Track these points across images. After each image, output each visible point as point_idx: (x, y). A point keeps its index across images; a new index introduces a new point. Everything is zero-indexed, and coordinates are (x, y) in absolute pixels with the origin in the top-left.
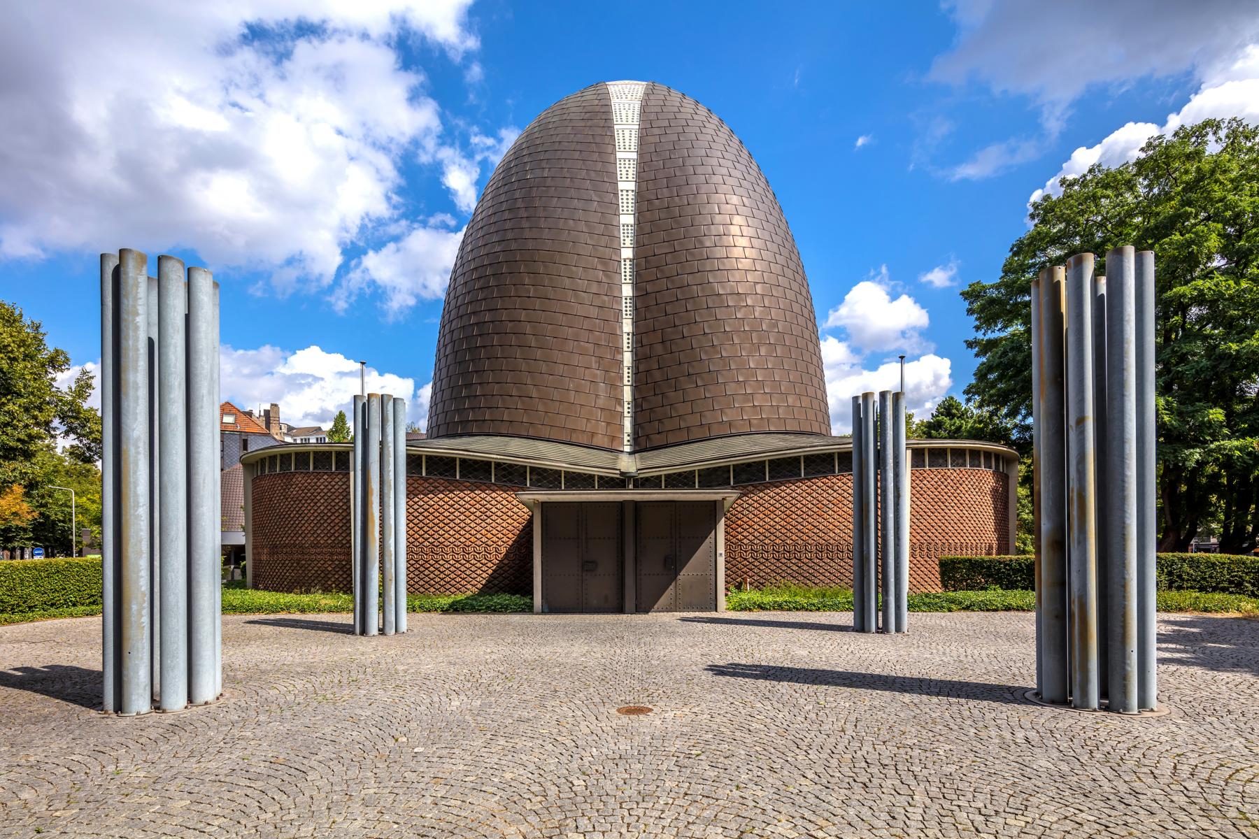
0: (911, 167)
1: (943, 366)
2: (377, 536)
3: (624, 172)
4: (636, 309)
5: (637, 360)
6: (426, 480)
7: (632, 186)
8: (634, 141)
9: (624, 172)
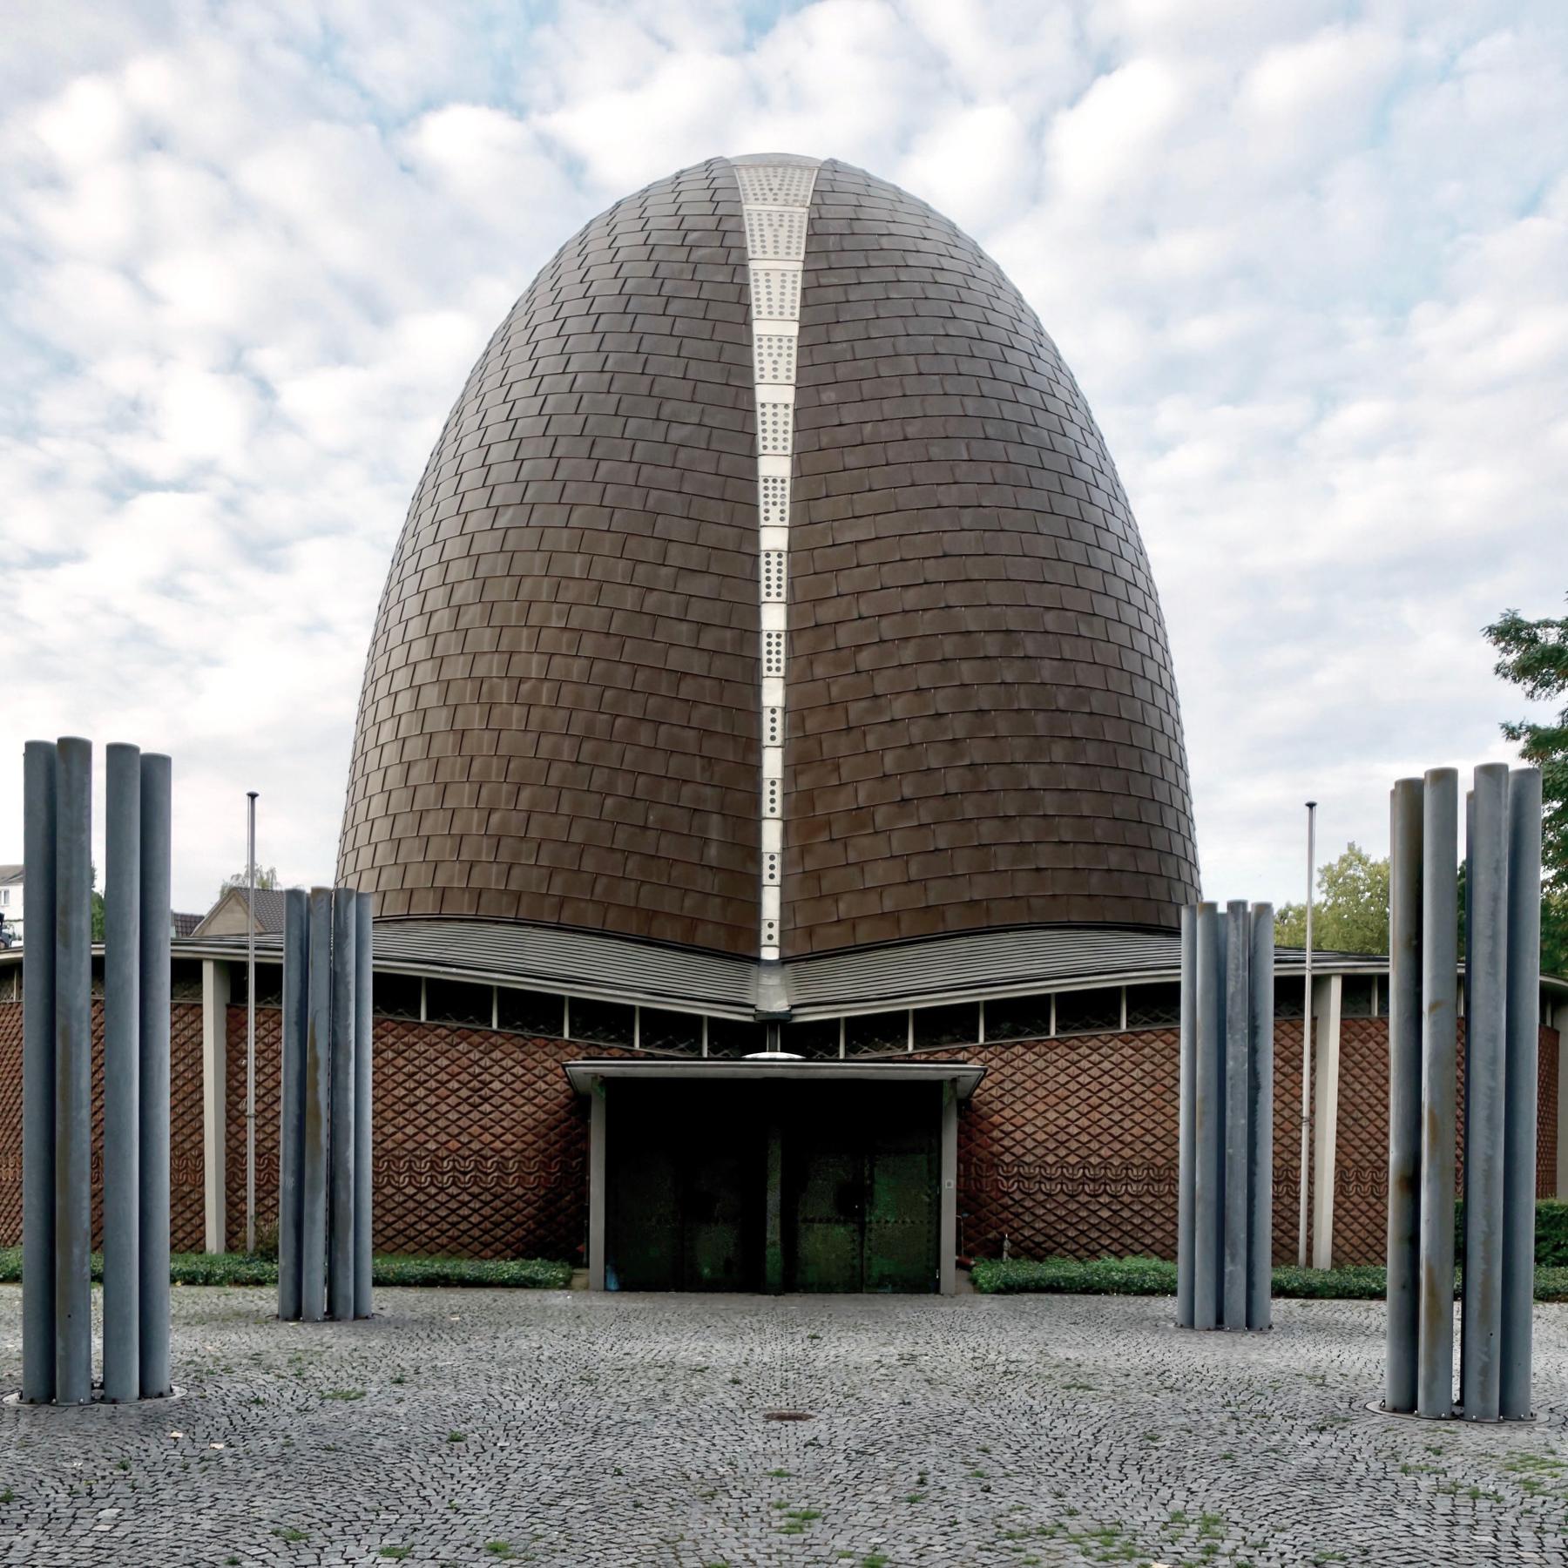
0: (706, 1271)
1: (94, 1290)
2: (324, 1141)
3: (768, 365)
4: (791, 657)
5: (792, 768)
6: (496, 1033)
7: (788, 395)
8: (793, 298)
9: (768, 365)
